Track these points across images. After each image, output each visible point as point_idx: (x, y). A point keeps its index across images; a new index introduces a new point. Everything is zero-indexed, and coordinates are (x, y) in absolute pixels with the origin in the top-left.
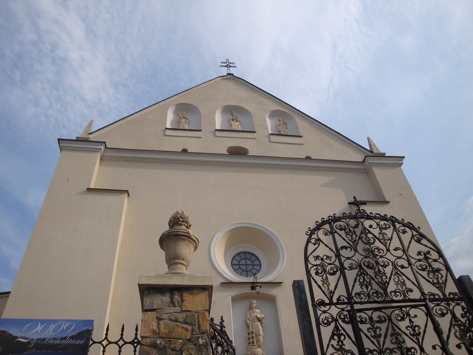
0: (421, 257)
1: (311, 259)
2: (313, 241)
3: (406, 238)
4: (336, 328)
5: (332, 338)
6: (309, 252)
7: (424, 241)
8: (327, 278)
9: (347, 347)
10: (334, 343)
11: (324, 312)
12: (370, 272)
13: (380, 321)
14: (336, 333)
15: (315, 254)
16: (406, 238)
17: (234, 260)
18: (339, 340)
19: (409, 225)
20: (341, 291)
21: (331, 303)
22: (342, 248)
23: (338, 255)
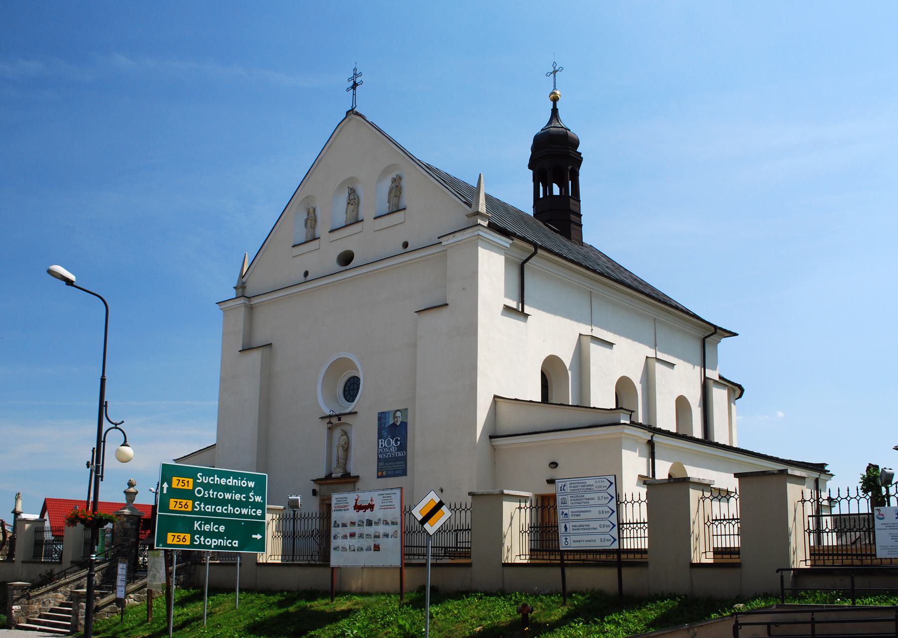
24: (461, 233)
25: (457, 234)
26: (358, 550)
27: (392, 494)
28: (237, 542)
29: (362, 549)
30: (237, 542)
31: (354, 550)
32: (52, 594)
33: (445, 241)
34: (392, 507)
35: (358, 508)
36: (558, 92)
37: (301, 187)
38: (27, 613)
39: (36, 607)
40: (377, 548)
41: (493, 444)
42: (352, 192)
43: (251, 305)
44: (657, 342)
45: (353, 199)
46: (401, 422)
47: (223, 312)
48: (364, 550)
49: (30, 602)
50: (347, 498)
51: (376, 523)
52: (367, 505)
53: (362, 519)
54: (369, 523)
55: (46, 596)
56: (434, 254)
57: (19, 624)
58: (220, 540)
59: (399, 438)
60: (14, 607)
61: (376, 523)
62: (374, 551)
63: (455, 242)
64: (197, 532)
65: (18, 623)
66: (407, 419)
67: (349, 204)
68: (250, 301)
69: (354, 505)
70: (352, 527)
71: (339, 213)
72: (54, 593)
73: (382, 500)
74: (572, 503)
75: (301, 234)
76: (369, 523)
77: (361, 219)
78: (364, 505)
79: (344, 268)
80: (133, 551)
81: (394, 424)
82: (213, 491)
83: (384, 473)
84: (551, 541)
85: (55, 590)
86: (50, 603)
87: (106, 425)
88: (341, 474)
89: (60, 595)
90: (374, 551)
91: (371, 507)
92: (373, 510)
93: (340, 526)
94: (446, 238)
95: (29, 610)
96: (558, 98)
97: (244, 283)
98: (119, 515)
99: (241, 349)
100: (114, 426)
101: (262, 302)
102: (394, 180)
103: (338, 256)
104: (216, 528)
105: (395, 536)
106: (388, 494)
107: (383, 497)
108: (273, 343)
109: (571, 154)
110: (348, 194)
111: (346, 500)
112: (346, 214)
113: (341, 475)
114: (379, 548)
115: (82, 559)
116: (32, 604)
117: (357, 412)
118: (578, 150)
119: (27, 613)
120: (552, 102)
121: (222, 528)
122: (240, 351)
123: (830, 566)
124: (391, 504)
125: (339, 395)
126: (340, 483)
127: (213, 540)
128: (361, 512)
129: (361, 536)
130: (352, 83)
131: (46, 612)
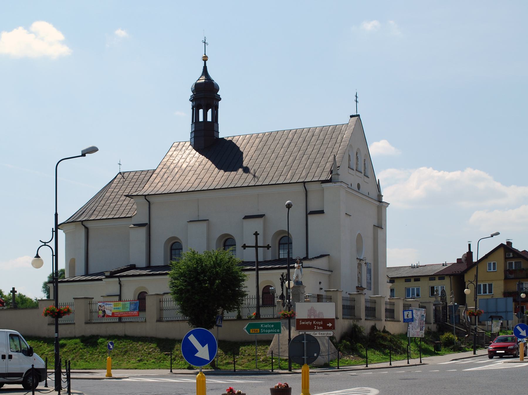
28: (279, 330)
30: (279, 330)
58: (271, 330)
64: (262, 328)
82: (310, 322)
84: (249, 299)
87: (52, 244)
100: (44, 244)
104: (270, 326)
109: (216, 97)
118: (218, 93)
121: (272, 326)
127: (269, 330)
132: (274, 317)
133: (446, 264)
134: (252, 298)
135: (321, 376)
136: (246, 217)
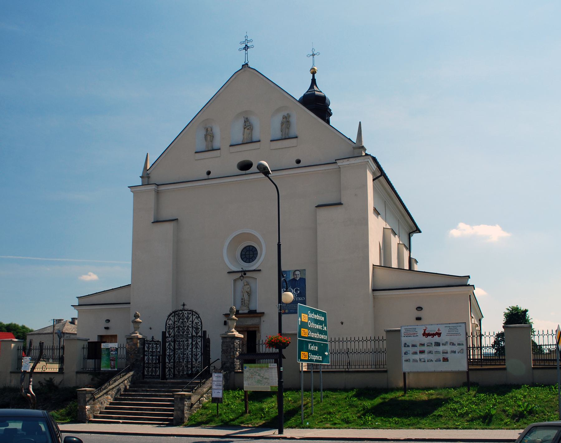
0: (196, 324)
1: (167, 324)
2: (169, 319)
3: (194, 317)
4: (170, 343)
5: (168, 345)
6: (167, 322)
7: (199, 319)
8: (170, 330)
9: (171, 348)
10: (168, 347)
11: (168, 339)
12: (181, 329)
13: (181, 342)
14: (170, 344)
15: (168, 323)
16: (194, 317)
17: (242, 256)
18: (170, 346)
19: (161, 355)
20: (173, 334)
21: (170, 337)
22: (176, 321)
23: (174, 323)
24: (354, 159)
25: (351, 159)
26: (428, 361)
27: (458, 326)
29: (432, 361)
31: (425, 362)
32: (106, 396)
33: (340, 163)
34: (457, 334)
35: (425, 334)
36: (316, 68)
37: (202, 112)
38: (94, 411)
39: (98, 406)
40: (445, 360)
41: (374, 295)
42: (247, 121)
43: (158, 190)
44: (400, 235)
45: (248, 125)
46: (300, 278)
47: (133, 193)
48: (434, 361)
49: (95, 403)
50: (416, 328)
51: (443, 344)
52: (435, 333)
53: (431, 342)
54: (438, 344)
55: (102, 397)
56: (325, 170)
57: (90, 419)
59: (299, 289)
60: (87, 407)
61: (443, 344)
62: (443, 361)
63: (348, 164)
65: (89, 418)
66: (305, 277)
67: (245, 128)
68: (158, 188)
69: (423, 333)
70: (421, 347)
71: (238, 134)
72: (106, 395)
73: (449, 330)
74: (449, 332)
75: (201, 145)
76: (438, 344)
77: (257, 140)
78: (432, 333)
79: (244, 172)
80: (142, 364)
81: (294, 280)
83: (286, 311)
84: (37, 348)
85: (106, 393)
86: (105, 403)
88: (248, 311)
89: (109, 397)
90: (443, 361)
91: (439, 334)
92: (440, 336)
93: (411, 346)
94: (342, 161)
95: (94, 409)
96: (316, 72)
97: (148, 174)
98: (131, 338)
99: (153, 221)
101: (168, 189)
102: (284, 117)
103: (238, 163)
105: (462, 352)
106: (453, 326)
107: (450, 328)
108: (178, 218)
110: (244, 122)
111: (415, 330)
112: (243, 135)
113: (248, 312)
114: (448, 360)
115: (82, 370)
116: (96, 404)
117: (260, 270)
119: (94, 411)
120: (312, 75)
122: (153, 222)
123: (552, 365)
124: (457, 332)
125: (238, 257)
126: (247, 317)
128: (430, 337)
129: (430, 352)
130: (244, 46)
131: (103, 409)
132: (483, 349)
133: (534, 331)
134: (36, 349)
135: (475, 304)
136: (196, 153)
